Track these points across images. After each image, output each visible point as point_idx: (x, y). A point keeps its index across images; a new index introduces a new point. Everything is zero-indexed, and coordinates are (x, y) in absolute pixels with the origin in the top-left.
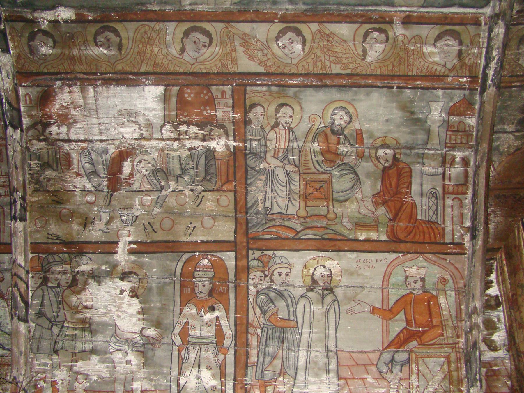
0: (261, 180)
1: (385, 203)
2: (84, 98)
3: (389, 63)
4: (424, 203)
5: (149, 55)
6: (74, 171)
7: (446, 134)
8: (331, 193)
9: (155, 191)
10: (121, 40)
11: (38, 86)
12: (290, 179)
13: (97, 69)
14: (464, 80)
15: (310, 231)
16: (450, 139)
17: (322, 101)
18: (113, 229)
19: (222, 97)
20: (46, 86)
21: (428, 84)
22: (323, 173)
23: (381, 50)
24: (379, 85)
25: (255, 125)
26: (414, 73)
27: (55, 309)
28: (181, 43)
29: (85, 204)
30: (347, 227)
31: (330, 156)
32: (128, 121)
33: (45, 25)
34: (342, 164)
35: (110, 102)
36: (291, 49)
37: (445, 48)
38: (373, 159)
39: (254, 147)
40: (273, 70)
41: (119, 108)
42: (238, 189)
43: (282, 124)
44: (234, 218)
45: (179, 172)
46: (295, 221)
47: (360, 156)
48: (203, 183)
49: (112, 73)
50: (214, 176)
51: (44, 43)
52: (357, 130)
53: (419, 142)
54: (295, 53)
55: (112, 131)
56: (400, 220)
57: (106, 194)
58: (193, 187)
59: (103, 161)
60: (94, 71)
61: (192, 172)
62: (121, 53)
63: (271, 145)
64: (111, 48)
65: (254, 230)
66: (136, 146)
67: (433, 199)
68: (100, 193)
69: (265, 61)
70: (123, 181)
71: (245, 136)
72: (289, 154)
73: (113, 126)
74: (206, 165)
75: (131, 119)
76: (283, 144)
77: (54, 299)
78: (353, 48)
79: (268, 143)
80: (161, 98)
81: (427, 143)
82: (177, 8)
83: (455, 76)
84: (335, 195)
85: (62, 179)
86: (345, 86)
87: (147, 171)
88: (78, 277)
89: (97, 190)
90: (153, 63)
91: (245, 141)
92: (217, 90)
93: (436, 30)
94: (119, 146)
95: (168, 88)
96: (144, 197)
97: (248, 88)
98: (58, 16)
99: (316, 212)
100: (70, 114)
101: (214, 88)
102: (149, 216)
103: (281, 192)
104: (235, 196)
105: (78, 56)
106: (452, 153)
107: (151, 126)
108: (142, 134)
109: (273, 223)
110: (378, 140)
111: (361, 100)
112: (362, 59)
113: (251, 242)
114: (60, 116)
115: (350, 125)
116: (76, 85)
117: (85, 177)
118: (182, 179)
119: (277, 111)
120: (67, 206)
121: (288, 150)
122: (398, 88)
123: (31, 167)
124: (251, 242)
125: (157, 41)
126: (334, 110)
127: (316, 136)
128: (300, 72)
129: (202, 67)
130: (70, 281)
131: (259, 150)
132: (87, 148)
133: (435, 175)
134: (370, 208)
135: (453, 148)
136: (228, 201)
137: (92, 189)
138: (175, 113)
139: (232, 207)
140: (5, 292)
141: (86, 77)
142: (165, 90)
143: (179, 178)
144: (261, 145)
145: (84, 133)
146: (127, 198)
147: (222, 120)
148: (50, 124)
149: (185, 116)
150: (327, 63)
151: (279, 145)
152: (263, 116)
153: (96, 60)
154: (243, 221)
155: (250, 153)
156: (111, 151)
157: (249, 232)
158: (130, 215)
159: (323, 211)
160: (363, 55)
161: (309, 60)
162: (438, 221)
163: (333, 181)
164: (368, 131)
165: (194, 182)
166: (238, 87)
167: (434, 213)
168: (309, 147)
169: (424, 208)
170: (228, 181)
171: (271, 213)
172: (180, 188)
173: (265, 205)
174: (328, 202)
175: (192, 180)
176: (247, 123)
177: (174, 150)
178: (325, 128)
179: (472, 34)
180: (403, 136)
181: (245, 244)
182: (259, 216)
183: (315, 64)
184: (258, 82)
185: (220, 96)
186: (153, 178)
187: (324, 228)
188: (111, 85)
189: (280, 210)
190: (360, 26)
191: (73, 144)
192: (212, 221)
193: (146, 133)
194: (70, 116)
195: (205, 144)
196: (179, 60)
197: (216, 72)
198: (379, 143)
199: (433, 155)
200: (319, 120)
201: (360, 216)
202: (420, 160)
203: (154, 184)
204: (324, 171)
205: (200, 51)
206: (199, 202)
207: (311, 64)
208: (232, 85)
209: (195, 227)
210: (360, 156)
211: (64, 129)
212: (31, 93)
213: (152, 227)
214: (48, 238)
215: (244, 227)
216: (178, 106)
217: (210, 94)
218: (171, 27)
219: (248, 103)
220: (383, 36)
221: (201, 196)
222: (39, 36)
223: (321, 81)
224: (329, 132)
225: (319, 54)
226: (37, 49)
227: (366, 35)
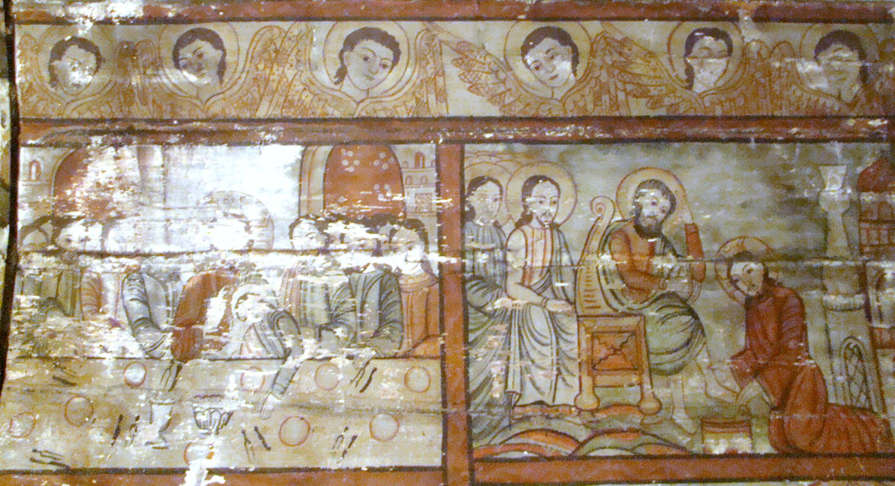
0: (496, 333)
1: (757, 372)
2: (143, 169)
3: (735, 94)
4: (837, 368)
5: (274, 85)
6: (108, 316)
7: (860, 229)
8: (644, 359)
9: (272, 358)
10: (224, 55)
11: (57, 145)
12: (558, 331)
13: (173, 112)
14: (877, 123)
15: (607, 441)
16: (868, 235)
17: (614, 170)
18: (178, 440)
19: (417, 165)
21: (812, 133)
22: (625, 315)
23: (720, 71)
24: (722, 135)
25: (482, 221)
26: (785, 112)
28: (338, 61)
29: (121, 386)
30: (685, 427)
31: (639, 281)
32: (226, 215)
33: (85, 30)
34: (663, 296)
35: (194, 176)
36: (550, 69)
37: (836, 64)
38: (726, 283)
39: (482, 266)
40: (517, 110)
41: (208, 189)
42: (449, 352)
43: (537, 218)
44: (441, 416)
45: (323, 319)
46: (573, 420)
47: (698, 278)
48: (377, 342)
49: (202, 121)
50: (398, 326)
51: (80, 64)
52: (686, 225)
53: (811, 246)
54: (560, 77)
55: (191, 233)
56: (795, 408)
57: (167, 364)
58: (353, 351)
59: (167, 297)
60: (167, 116)
61: (351, 318)
62: (221, 81)
63: (516, 261)
64: (203, 71)
65: (486, 441)
66: (237, 265)
67: (855, 360)
68: (156, 364)
69: (501, 94)
70: (206, 337)
71: (463, 243)
72: (554, 278)
73: (194, 225)
74: (380, 303)
75: (232, 211)
76: (539, 256)
78: (669, 67)
79: (510, 257)
80: (294, 169)
81: (825, 249)
83: (861, 117)
84: (654, 360)
85: (79, 333)
86: (658, 140)
87: (257, 316)
89: (151, 356)
90: (282, 99)
91: (462, 254)
92: (407, 151)
93: (815, 33)
94: (203, 265)
95: (309, 148)
96: (249, 373)
97: (468, 147)
98: (112, 11)
99: (618, 399)
100: (111, 200)
101: (399, 149)
102: (257, 415)
103: (539, 357)
104: (443, 369)
105: (140, 86)
106: (875, 264)
107: (270, 225)
108: (252, 241)
109: (525, 426)
110: (730, 244)
111: (690, 167)
112: (686, 88)
113: (480, 467)
115: (672, 217)
116: (129, 143)
117: (128, 330)
118: (329, 333)
119: (527, 190)
120: (83, 391)
121: (551, 271)
122: (757, 141)
123: (19, 308)
124: (480, 467)
125: (293, 57)
126: (639, 187)
127: (606, 241)
128: (570, 115)
129: (378, 107)
131: (491, 271)
132: (138, 270)
133: (851, 310)
134: (728, 384)
135: (878, 254)
136: (427, 379)
137: (140, 354)
138: (320, 197)
139: (436, 392)
141: (150, 127)
142: (304, 154)
143: (324, 332)
144: (495, 262)
145: (135, 240)
146: (212, 374)
147: (417, 210)
148: (69, 221)
149: (341, 205)
150: (621, 96)
151: (532, 262)
152: (498, 202)
153: (172, 96)
154: (461, 424)
155: (474, 277)
156: (185, 277)
157: (475, 445)
158: (216, 410)
159: (632, 396)
160: (687, 80)
161: (587, 91)
162: (871, 406)
163: (649, 330)
164: (708, 227)
165: (354, 340)
166: (449, 146)
167: (861, 391)
168: (595, 262)
169: (838, 380)
170: (427, 337)
171: (521, 403)
172: (325, 353)
173: (506, 387)
174: (640, 374)
175: (351, 336)
176: (466, 216)
177: (315, 273)
178: (623, 224)
179: (881, 38)
180: (778, 234)
181: (466, 473)
182: (494, 411)
183: (597, 99)
184: (488, 136)
185: (412, 163)
186: (269, 332)
187: (636, 431)
188: (197, 144)
189: (539, 397)
190: (678, 26)
191: (110, 261)
192: (392, 425)
193: (259, 239)
194: (110, 205)
195: (380, 260)
196: (335, 93)
197: (405, 116)
198: (731, 250)
199: (840, 270)
200: (610, 208)
201: (710, 403)
202: (817, 281)
203: (271, 344)
204: (627, 311)
205: (375, 76)
206: (364, 381)
207: (589, 99)
208: (436, 142)
209: (354, 438)
210: (698, 278)
211: (96, 231)
212: (43, 158)
213: (261, 437)
214: (33, 460)
215: (463, 436)
216: (329, 184)
217: (392, 160)
219: (468, 177)
220: (722, 44)
221: (368, 370)
222: (74, 50)
223: (610, 130)
224: (631, 230)
225: (604, 77)
226: (66, 74)
227: (691, 41)
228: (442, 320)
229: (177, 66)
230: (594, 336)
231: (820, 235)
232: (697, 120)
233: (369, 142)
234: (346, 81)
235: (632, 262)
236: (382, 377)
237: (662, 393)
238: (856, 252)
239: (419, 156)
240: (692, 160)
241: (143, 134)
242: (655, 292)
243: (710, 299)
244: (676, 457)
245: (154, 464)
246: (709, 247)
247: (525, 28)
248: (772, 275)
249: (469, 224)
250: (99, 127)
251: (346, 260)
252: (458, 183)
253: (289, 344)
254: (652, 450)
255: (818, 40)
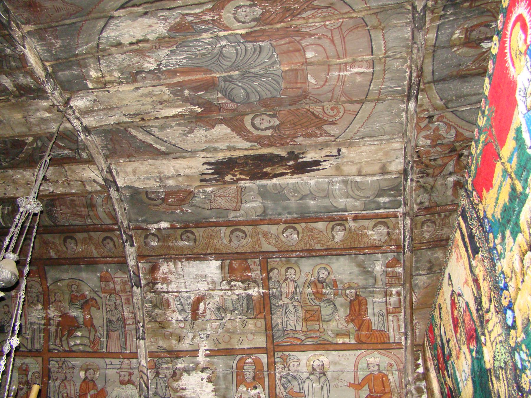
1: (352, 321)
2: (176, 268)
4: (376, 319)
11: (150, 262)
13: (182, 252)
14: (393, 247)
15: (310, 340)
17: (311, 265)
19: (254, 265)
20: (154, 262)
22: (315, 305)
23: (342, 235)
24: (344, 254)
27: (164, 391)
41: (196, 273)
47: (336, 294)
55: (192, 286)
58: (241, 317)
61: (239, 308)
63: (284, 291)
67: (381, 317)
77: (163, 385)
82: (226, 219)
84: (323, 318)
85: (165, 314)
86: (324, 256)
88: (176, 371)
89: (185, 320)
93: (372, 222)
97: (268, 260)
101: (249, 261)
114: (162, 278)
121: (294, 293)
122: (355, 254)
124: (276, 347)
130: (172, 374)
135: (391, 286)
137: (182, 319)
138: (228, 275)
139: (264, 327)
140: (135, 381)
142: (222, 263)
145: (177, 288)
147: (255, 278)
148: (157, 283)
153: (182, 248)
159: (317, 327)
165: (241, 314)
169: (376, 323)
170: (260, 313)
172: (233, 318)
176: (269, 279)
177: (228, 296)
180: (360, 281)
181: (272, 349)
183: (306, 244)
185: (253, 265)
189: (291, 328)
192: (252, 336)
195: (246, 292)
198: (346, 286)
202: (372, 295)
206: (244, 325)
207: (303, 245)
211: (165, 286)
215: (271, 339)
218: (223, 229)
219: (269, 268)
220: (343, 227)
221: (245, 322)
223: (310, 254)
226: (149, 243)
228: (264, 308)
229: (182, 240)
230: (306, 311)
231: (374, 281)
232: (336, 249)
233: (240, 259)
234: (232, 243)
235: (317, 291)
236: (249, 324)
237: (325, 327)
238: (384, 286)
239: (255, 263)
240: (334, 261)
241: (175, 259)
242: (324, 299)
243: (339, 301)
244: (328, 344)
245: (190, 349)
246: (340, 286)
247: (283, 226)
248: (358, 293)
249: (270, 281)
250: (161, 257)
251: (237, 292)
252: (266, 269)
253: (223, 315)
254: (321, 342)
255: (373, 224)
